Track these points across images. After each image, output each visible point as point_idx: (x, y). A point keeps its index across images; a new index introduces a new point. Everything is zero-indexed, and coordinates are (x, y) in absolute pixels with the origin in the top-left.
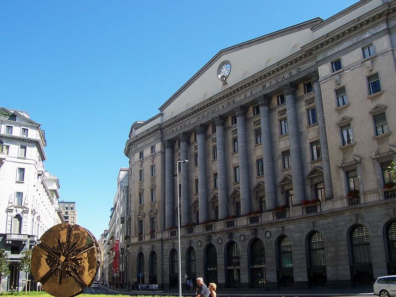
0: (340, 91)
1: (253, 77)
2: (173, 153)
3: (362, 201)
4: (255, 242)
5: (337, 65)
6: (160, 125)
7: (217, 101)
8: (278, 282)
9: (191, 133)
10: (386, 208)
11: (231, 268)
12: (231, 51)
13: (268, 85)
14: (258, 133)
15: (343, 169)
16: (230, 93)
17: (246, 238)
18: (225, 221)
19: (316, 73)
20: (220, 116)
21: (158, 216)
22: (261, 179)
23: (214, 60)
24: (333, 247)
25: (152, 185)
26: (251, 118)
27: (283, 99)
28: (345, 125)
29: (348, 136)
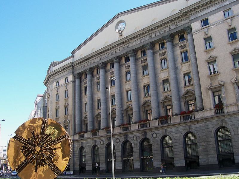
0: (208, 39)
2: (81, 82)
3: (225, 111)
4: (126, 143)
5: (205, 22)
6: (72, 63)
7: (115, 46)
8: (92, 170)
9: (94, 69)
10: (185, 126)
11: (126, 158)
12: (126, 14)
13: (153, 36)
14: (145, 68)
16: (126, 41)
17: (138, 138)
18: (122, 127)
19: (189, 29)
20: (117, 57)
21: (70, 124)
22: (148, 99)
23: (113, 19)
25: (66, 104)
26: (140, 58)
27: (163, 45)
28: (212, 61)
29: (214, 69)
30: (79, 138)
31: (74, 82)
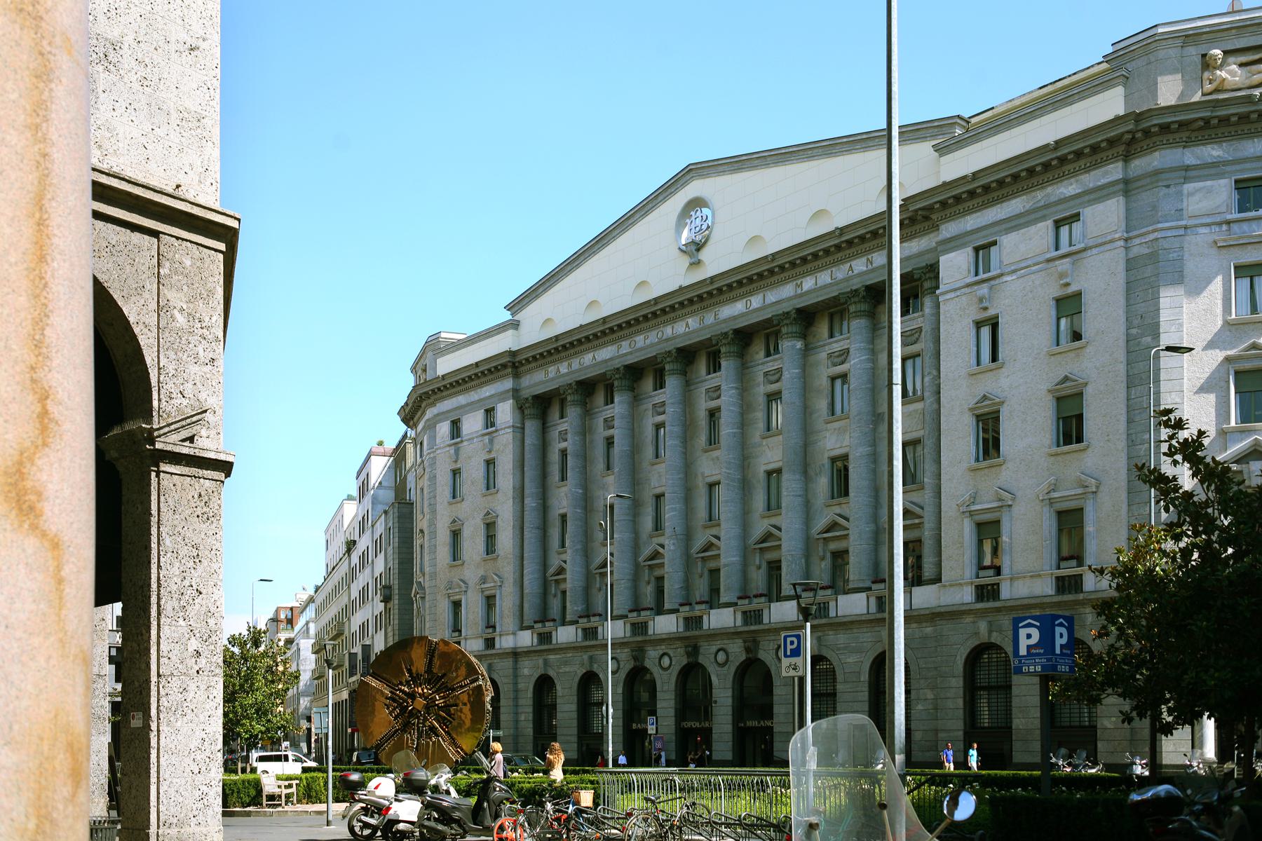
1: (773, 260)
6: (513, 354)
15: (971, 515)
24: (932, 689)
30: (579, 639)
31: (520, 430)
